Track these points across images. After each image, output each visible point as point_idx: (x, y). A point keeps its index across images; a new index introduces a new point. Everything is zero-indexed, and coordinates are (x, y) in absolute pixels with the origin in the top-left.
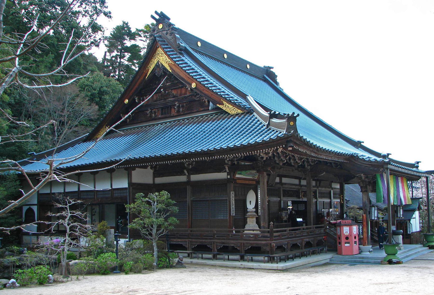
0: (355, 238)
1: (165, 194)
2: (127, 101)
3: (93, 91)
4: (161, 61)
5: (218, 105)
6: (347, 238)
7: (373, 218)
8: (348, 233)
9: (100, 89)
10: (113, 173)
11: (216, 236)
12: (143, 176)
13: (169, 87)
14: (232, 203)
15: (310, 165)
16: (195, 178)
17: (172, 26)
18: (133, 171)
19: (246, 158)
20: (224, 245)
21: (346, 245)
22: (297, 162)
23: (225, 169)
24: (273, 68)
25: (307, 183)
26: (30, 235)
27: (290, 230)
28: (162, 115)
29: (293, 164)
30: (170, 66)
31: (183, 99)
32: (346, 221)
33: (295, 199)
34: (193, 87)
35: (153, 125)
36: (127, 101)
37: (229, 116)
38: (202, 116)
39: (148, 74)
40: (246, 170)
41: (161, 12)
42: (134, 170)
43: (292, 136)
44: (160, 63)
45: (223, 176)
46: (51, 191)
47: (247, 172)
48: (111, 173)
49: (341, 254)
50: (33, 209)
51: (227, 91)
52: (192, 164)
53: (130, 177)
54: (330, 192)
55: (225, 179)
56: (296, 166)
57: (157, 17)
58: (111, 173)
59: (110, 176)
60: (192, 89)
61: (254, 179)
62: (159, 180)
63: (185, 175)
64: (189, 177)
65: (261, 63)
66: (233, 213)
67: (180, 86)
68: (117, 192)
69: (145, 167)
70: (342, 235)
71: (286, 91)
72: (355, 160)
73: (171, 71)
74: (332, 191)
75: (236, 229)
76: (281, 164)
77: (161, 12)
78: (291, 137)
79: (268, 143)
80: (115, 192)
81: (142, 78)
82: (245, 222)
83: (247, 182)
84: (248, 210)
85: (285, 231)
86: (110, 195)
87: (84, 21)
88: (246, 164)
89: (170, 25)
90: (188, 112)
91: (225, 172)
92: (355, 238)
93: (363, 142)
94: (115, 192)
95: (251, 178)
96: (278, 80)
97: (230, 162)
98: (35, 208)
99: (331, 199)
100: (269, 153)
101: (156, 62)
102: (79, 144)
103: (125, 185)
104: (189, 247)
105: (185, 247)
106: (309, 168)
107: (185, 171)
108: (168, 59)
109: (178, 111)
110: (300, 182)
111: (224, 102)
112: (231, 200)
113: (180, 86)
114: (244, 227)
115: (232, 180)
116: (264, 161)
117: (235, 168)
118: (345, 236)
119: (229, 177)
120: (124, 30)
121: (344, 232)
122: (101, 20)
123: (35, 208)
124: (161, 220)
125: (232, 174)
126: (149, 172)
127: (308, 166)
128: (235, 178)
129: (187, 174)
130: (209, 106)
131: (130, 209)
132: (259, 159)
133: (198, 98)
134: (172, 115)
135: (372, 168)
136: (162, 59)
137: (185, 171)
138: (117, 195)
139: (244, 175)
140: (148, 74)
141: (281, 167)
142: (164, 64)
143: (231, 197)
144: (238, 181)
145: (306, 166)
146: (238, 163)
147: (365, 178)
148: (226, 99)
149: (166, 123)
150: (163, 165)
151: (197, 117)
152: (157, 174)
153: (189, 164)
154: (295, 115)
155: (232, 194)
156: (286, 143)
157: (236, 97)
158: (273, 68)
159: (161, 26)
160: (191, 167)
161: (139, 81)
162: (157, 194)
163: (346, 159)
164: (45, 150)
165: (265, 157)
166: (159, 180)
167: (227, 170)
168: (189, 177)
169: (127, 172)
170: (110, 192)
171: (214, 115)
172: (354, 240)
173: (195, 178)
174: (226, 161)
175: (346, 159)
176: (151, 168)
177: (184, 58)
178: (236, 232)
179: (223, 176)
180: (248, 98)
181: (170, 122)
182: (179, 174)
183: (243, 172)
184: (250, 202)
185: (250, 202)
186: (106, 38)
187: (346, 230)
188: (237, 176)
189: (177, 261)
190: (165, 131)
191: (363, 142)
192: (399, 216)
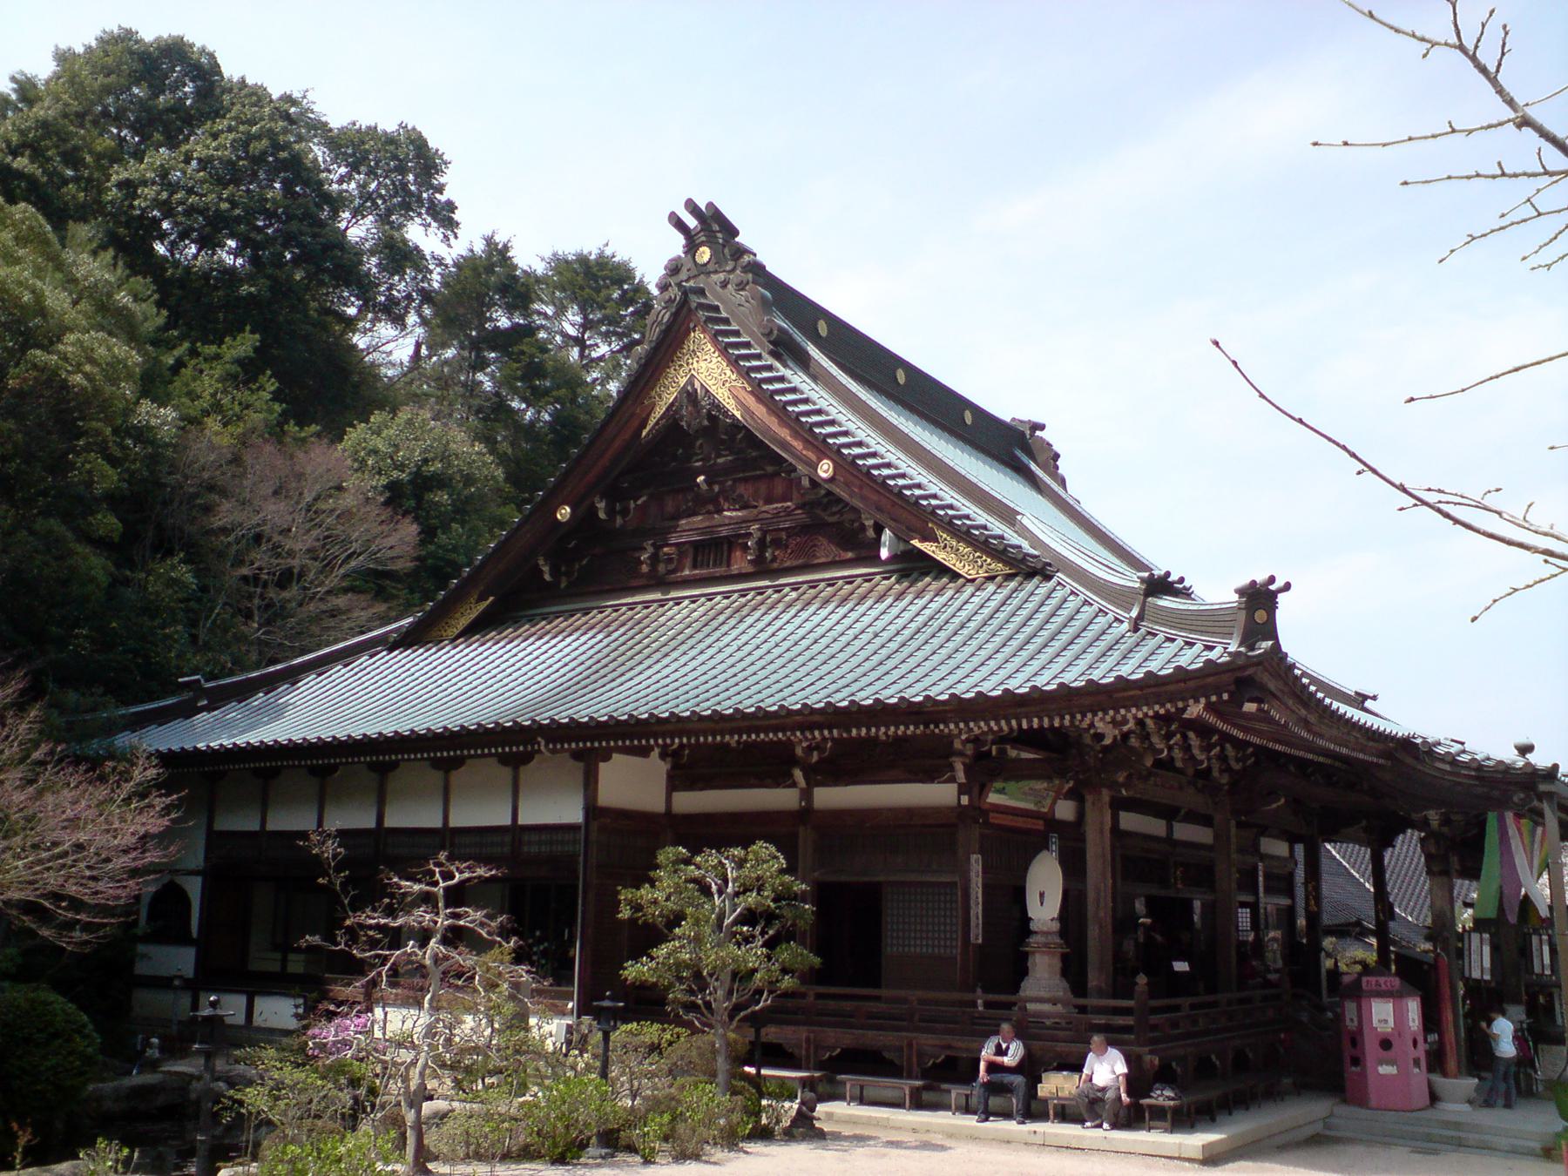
0: (1415, 1043)
1: (766, 859)
2: (564, 513)
3: (395, 474)
4: (702, 377)
5: (916, 543)
6: (1386, 1044)
7: (1476, 974)
8: (1391, 1023)
9: (419, 468)
10: (522, 769)
11: (916, 1018)
12: (632, 784)
13: (727, 470)
14: (973, 897)
15: (1229, 770)
16: (830, 797)
17: (746, 258)
18: (601, 765)
19: (1042, 733)
20: (948, 1053)
21: (1384, 1070)
22: (1192, 757)
23: (952, 768)
24: (1042, 427)
25: (1216, 837)
26: (175, 988)
27: (1193, 1007)
28: (695, 567)
29: (1179, 764)
30: (735, 397)
31: (777, 515)
32: (1382, 980)
33: (1155, 891)
34: (824, 475)
35: (662, 603)
36: (564, 513)
37: (961, 581)
38: (849, 580)
39: (652, 422)
40: (1018, 777)
41: (710, 205)
42: (607, 758)
43: (1260, 661)
44: (697, 385)
45: (940, 794)
46: (263, 822)
47: (1021, 784)
48: (516, 769)
49: (1361, 1101)
50: (187, 887)
51: (949, 495)
52: (819, 747)
53: (590, 783)
54: (1255, 869)
55: (951, 809)
56: (1190, 771)
57: (692, 222)
58: (516, 769)
59: (509, 782)
60: (815, 483)
61: (1038, 812)
62: (690, 801)
63: (794, 785)
64: (807, 795)
65: (1004, 410)
66: (977, 936)
67: (770, 469)
68: (534, 837)
69: (644, 752)
70: (1366, 1030)
71: (1091, 508)
72: (1417, 758)
73: (738, 414)
74: (1260, 866)
75: (991, 997)
76: (1149, 762)
77: (710, 205)
78: (1259, 664)
79: (1164, 684)
80: (526, 838)
81: (627, 435)
82: (1023, 972)
83: (1020, 822)
84: (1033, 926)
85: (1177, 1008)
86: (507, 850)
87: (359, 231)
88: (1025, 755)
89: (741, 251)
90: (795, 563)
91: (952, 780)
92: (1415, 1043)
93: (1374, 698)
94: (526, 838)
95: (1031, 806)
96: (1064, 467)
97: (970, 746)
98: (194, 888)
99: (1256, 893)
100: (1125, 721)
101: (683, 381)
102: (371, 657)
103: (570, 811)
104: (808, 1057)
105: (891, 1063)
106: (1225, 780)
107: (798, 774)
108: (729, 373)
109: (759, 560)
110: (1170, 829)
111: (939, 533)
112: (973, 885)
113: (770, 469)
114: (1016, 988)
115: (975, 814)
116: (1106, 749)
117: (986, 768)
118: (1378, 1034)
119: (965, 800)
120: (493, 272)
121: (1375, 1023)
122: (420, 234)
123: (194, 888)
124: (754, 955)
125: (976, 790)
126: (655, 768)
127: (1221, 771)
128: (985, 807)
129: (802, 783)
130: (877, 543)
131: (637, 908)
132: (1087, 740)
133: (834, 514)
134: (735, 569)
135: (1480, 790)
136: (707, 371)
137: (798, 774)
138: (534, 849)
139: (1012, 797)
140: (652, 422)
141: (1150, 774)
142: (713, 390)
143: (973, 874)
144: (996, 819)
145: (1216, 774)
146: (1002, 752)
147: (1441, 825)
148: (950, 523)
149: (710, 597)
150: (716, 749)
151: (831, 582)
152: (684, 774)
153: (809, 747)
154: (1273, 587)
155: (976, 863)
156: (1233, 688)
157: (981, 517)
158: (1042, 427)
159: (704, 254)
160: (815, 757)
161: (618, 443)
162: (737, 852)
163: (1388, 755)
164: (231, 673)
165: (1110, 734)
166: (690, 801)
167: (961, 776)
168: (807, 795)
169: (581, 765)
170: (508, 839)
171: (859, 580)
172: (1413, 1053)
173: (830, 797)
174: (957, 745)
175: (1388, 755)
176: (663, 756)
177: (788, 373)
178: (987, 1005)
179: (940, 794)
180: (1025, 521)
181: (726, 595)
182: (769, 781)
183: (1012, 786)
184: (1042, 895)
185: (1042, 895)
186: (427, 297)
187: (1382, 1014)
188: (993, 798)
189: (793, 1113)
190: (715, 624)
191: (1374, 698)
192: (1537, 969)
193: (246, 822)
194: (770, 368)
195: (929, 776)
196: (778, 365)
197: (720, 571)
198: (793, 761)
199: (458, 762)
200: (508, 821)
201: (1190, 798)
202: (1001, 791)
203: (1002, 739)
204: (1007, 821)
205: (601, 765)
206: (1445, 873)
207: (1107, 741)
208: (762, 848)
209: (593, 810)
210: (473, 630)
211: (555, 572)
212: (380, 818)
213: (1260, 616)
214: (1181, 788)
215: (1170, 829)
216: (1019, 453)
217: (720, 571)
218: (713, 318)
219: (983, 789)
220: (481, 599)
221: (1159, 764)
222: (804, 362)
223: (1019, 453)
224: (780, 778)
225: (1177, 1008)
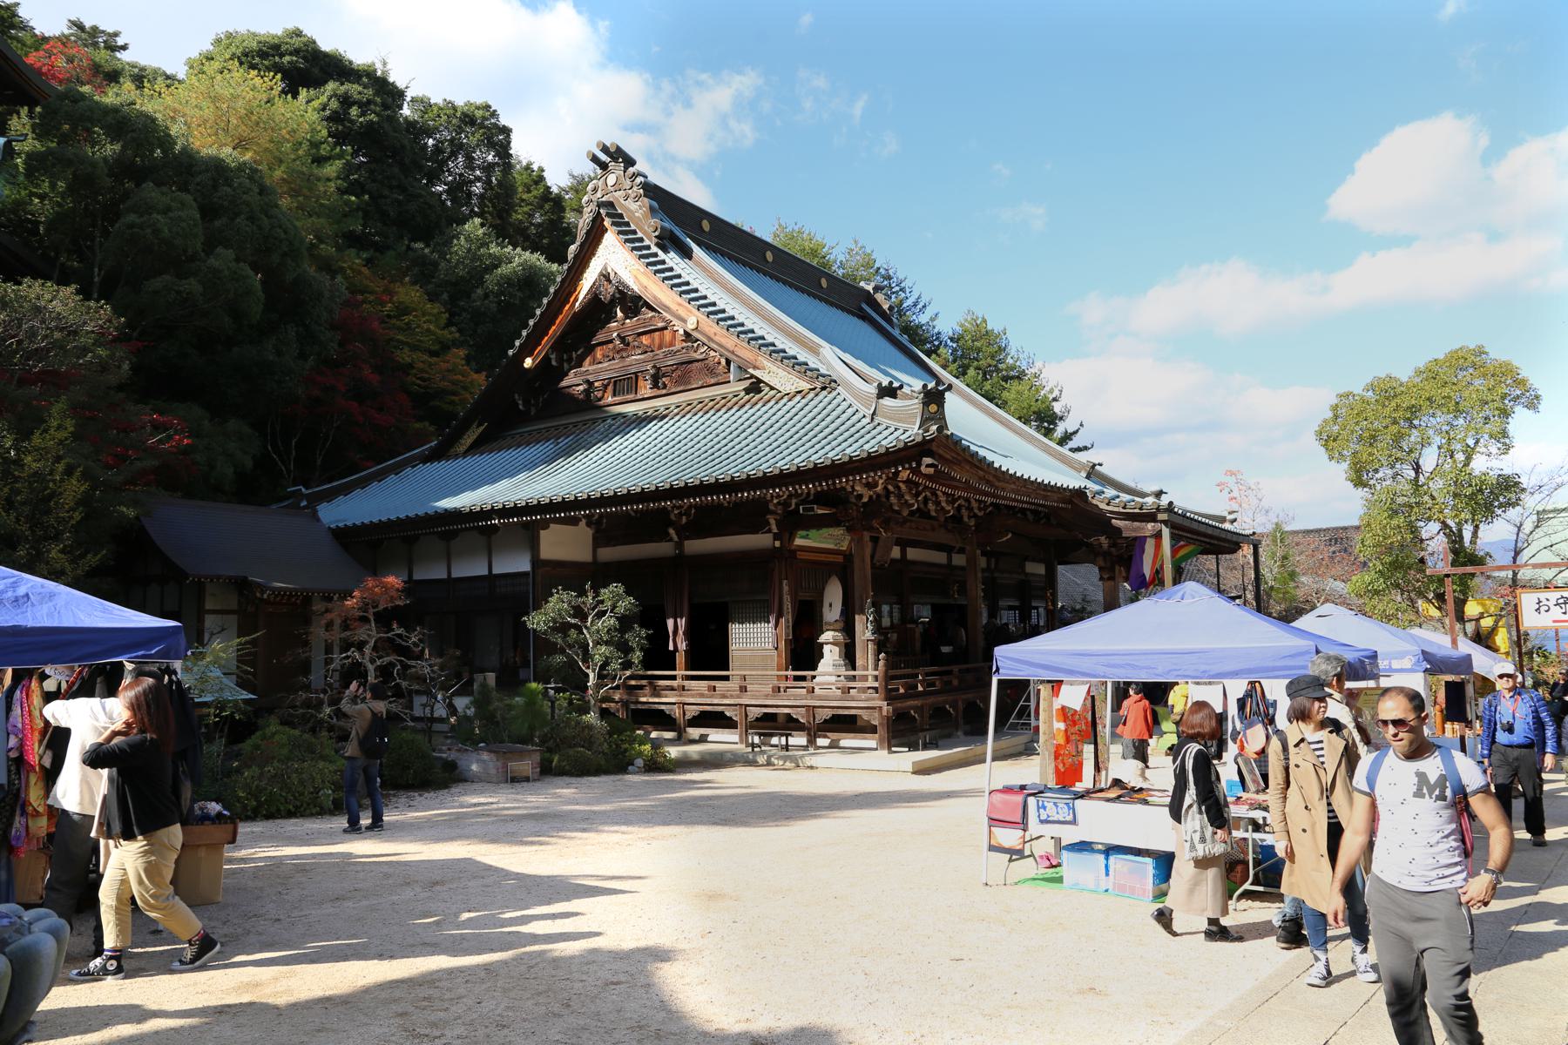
15: (975, 516)
16: (696, 546)
18: (542, 532)
53: (534, 546)
57: (603, 157)
62: (608, 554)
64: (679, 545)
69: (574, 521)
83: (822, 557)
85: (950, 673)
91: (769, 531)
95: (831, 546)
110: (950, 559)
117: (793, 522)
119: (777, 544)
126: (584, 532)
129: (675, 538)
144: (801, 555)
160: (684, 519)
168: (679, 545)
173: (696, 546)
176: (588, 525)
183: (813, 533)
188: (798, 542)
193: (439, 573)
194: (656, 255)
195: (755, 530)
196: (660, 253)
197: (631, 397)
198: (671, 524)
199: (455, 534)
200: (485, 572)
201: (942, 537)
202: (806, 537)
203: (805, 500)
204: (812, 556)
205: (542, 532)
206: (1112, 578)
207: (865, 500)
208: (616, 588)
209: (536, 562)
210: (477, 447)
211: (527, 402)
212: (449, 573)
213: (933, 408)
214: (933, 529)
215: (950, 559)
216: (864, 306)
217: (631, 397)
218: (619, 221)
219: (792, 537)
220: (480, 425)
221: (912, 513)
222: (686, 254)
223: (864, 306)
224: (758, 526)
225: (950, 673)
